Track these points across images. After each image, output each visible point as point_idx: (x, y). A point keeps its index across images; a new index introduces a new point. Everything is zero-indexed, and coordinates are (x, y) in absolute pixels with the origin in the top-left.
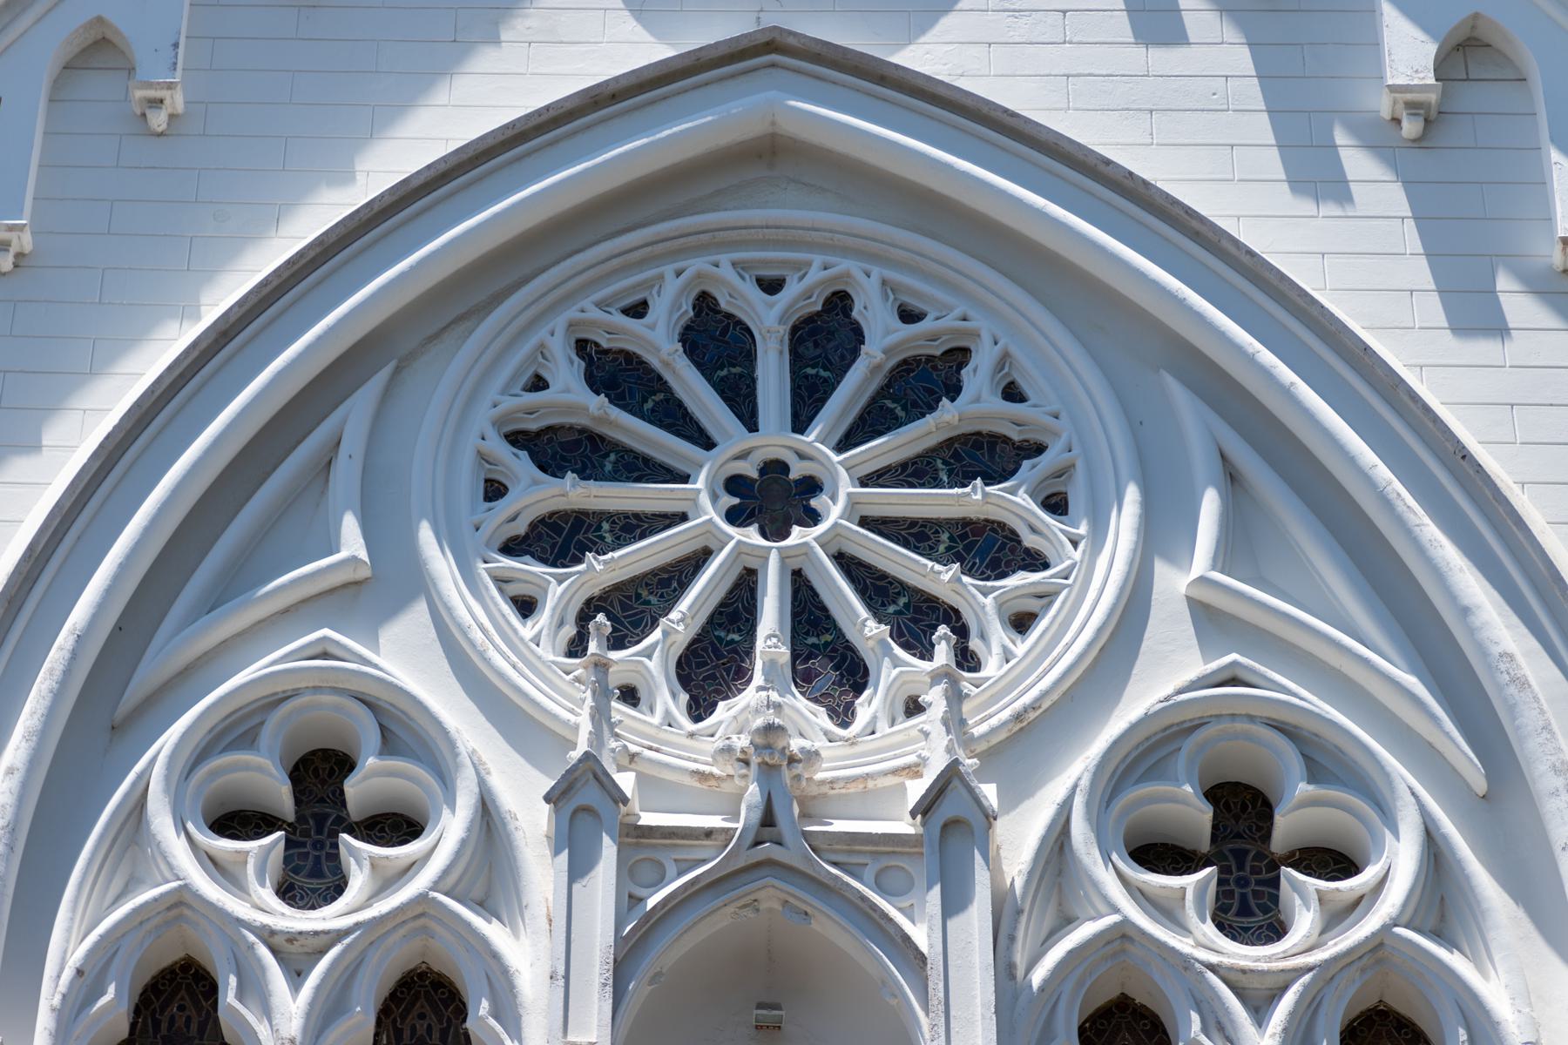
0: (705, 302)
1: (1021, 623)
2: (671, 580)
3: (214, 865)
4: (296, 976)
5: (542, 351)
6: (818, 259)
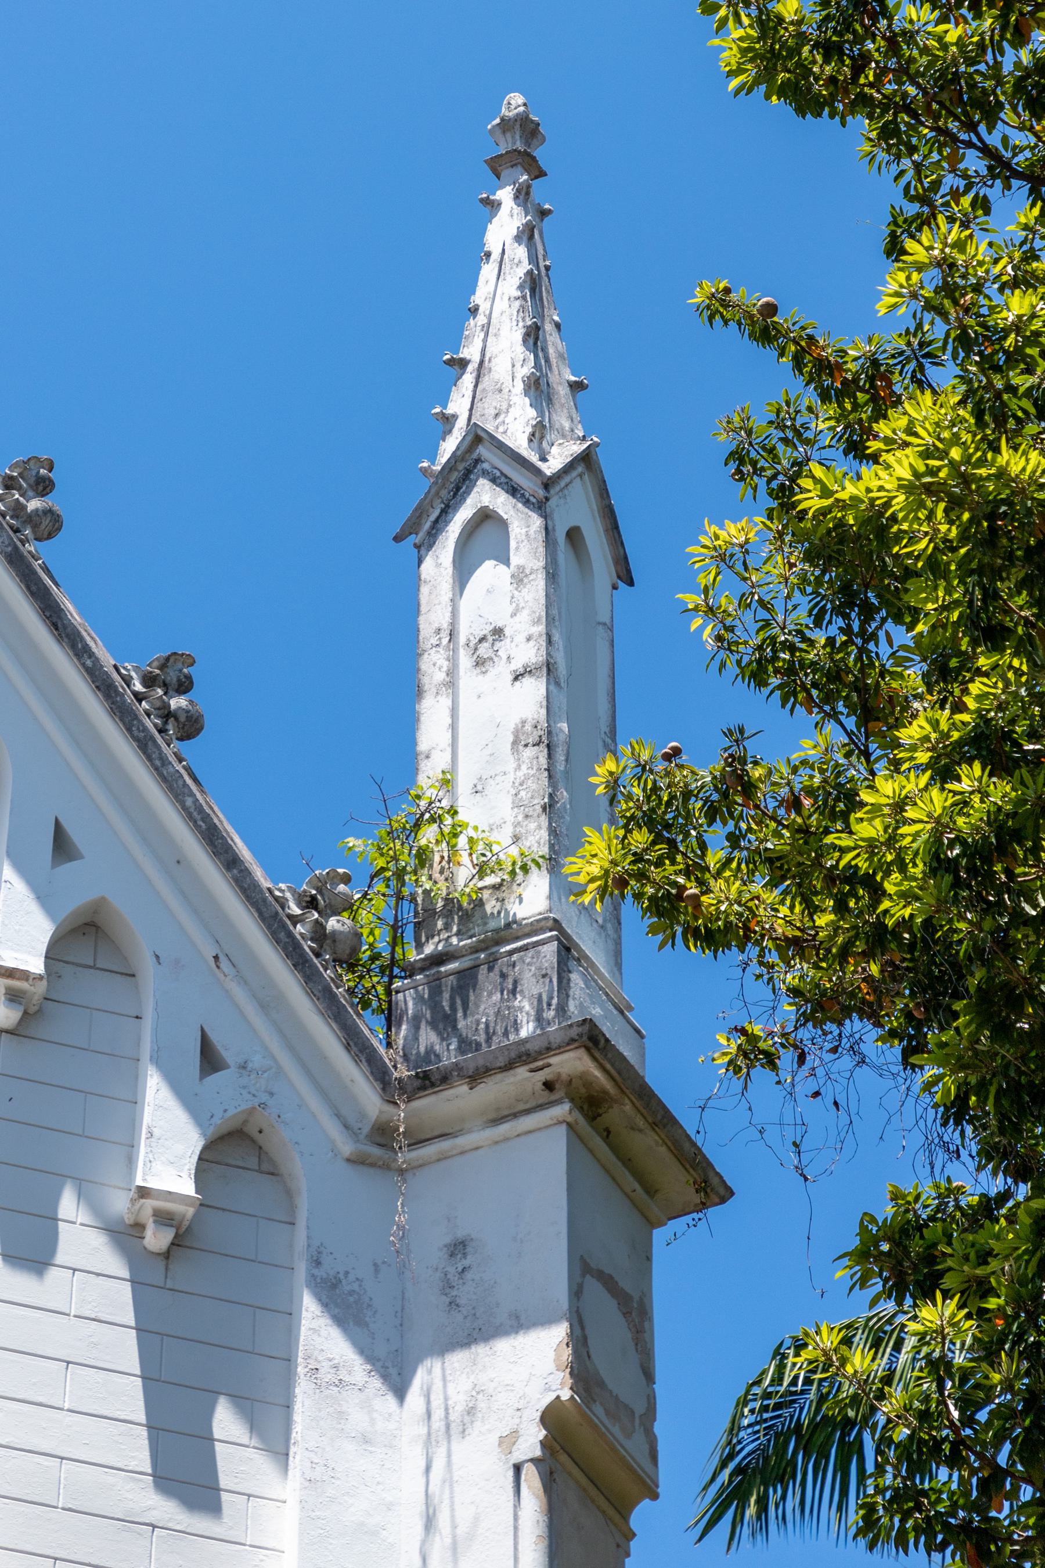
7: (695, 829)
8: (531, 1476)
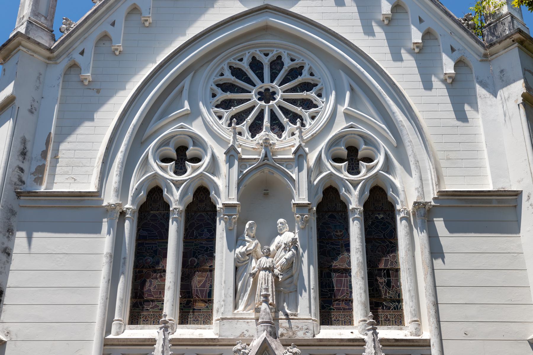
1: (313, 118)
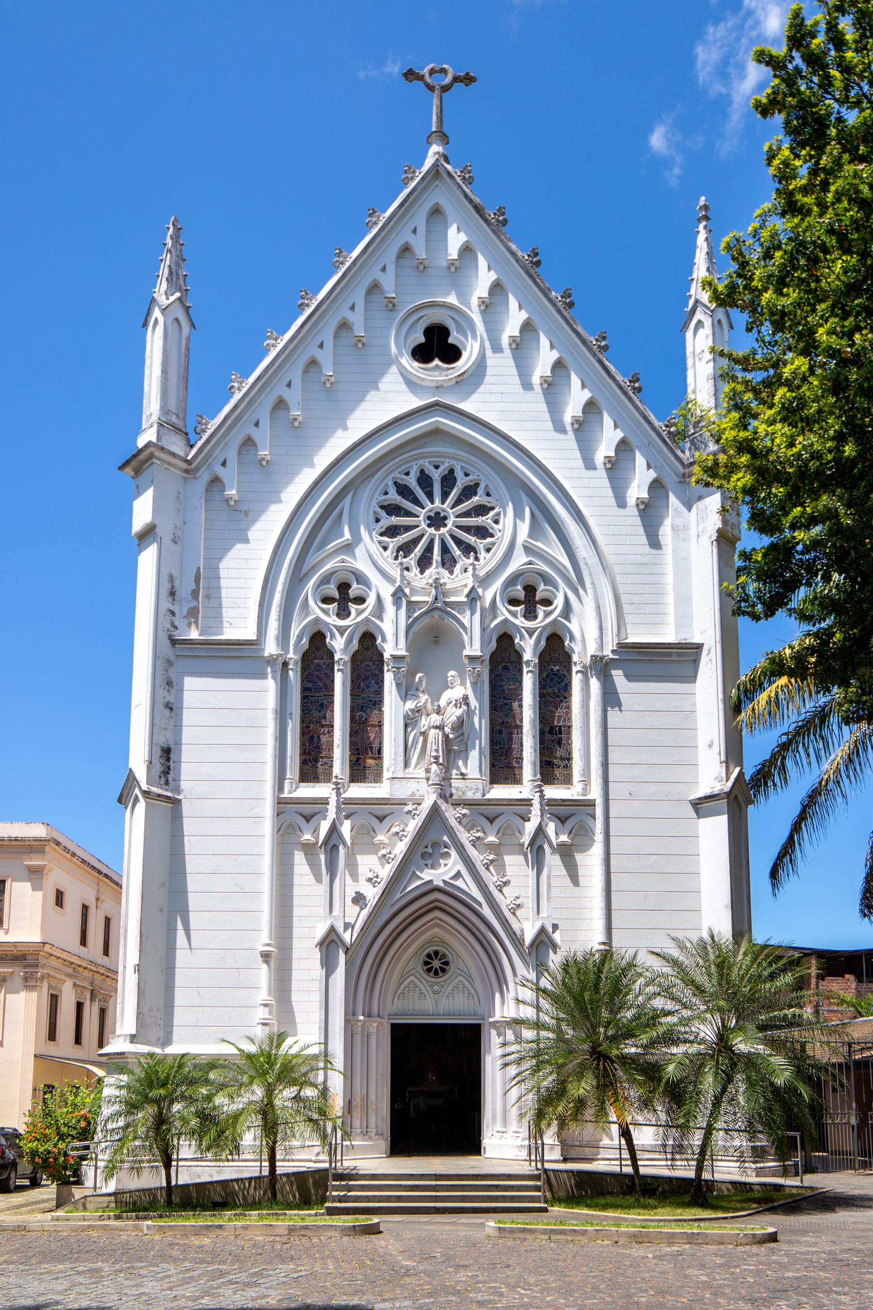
0: (422, 471)
1: (488, 550)
2: (416, 541)
3: (323, 610)
4: (342, 635)
5: (387, 485)
6: (447, 460)
7: (65, 1169)
8: (715, 543)
